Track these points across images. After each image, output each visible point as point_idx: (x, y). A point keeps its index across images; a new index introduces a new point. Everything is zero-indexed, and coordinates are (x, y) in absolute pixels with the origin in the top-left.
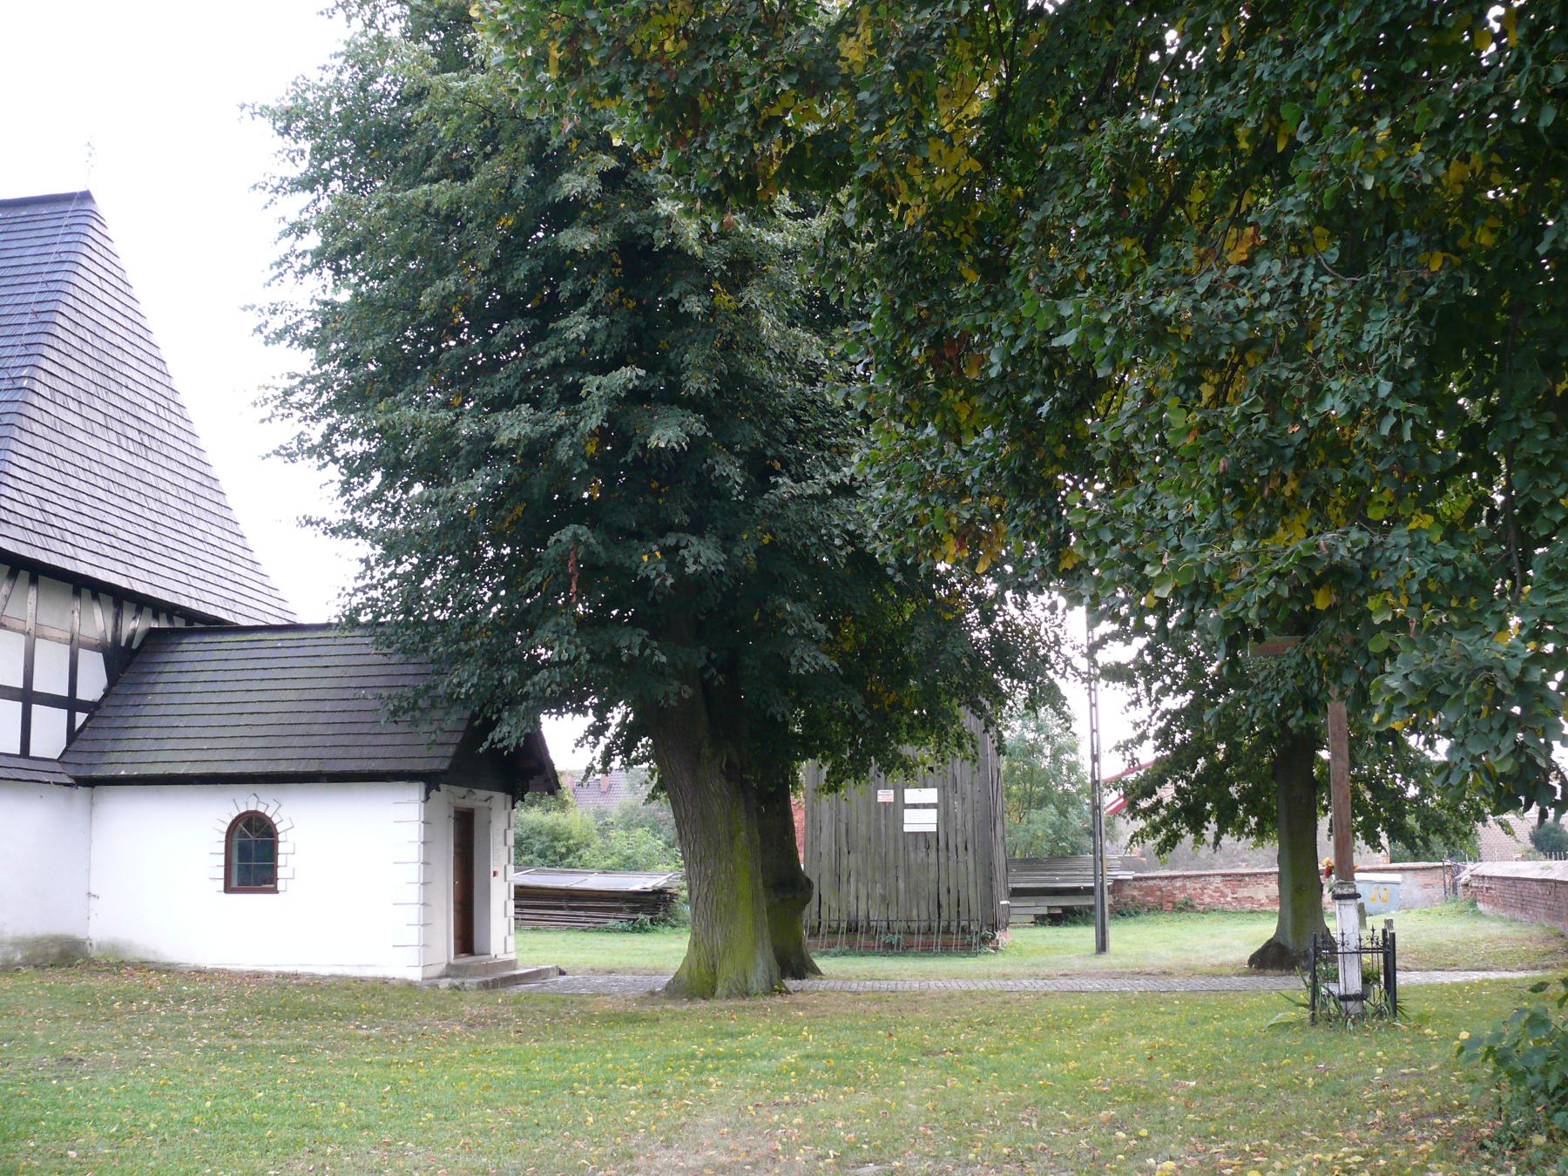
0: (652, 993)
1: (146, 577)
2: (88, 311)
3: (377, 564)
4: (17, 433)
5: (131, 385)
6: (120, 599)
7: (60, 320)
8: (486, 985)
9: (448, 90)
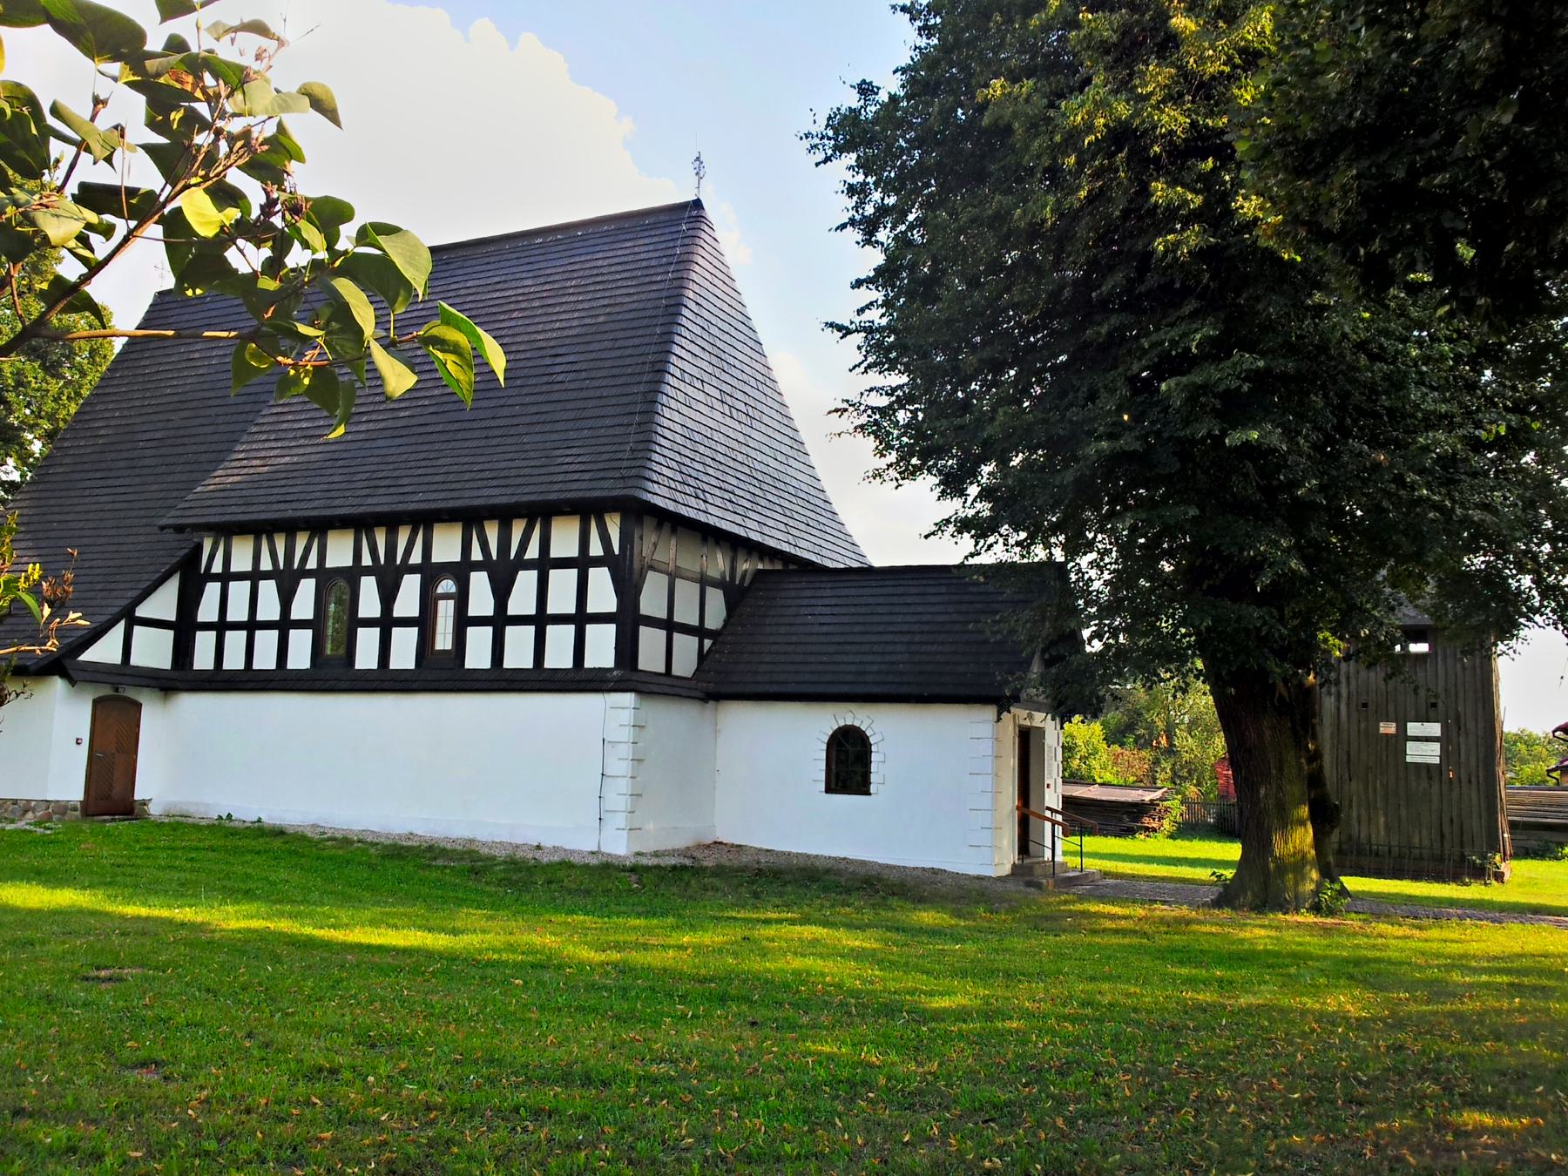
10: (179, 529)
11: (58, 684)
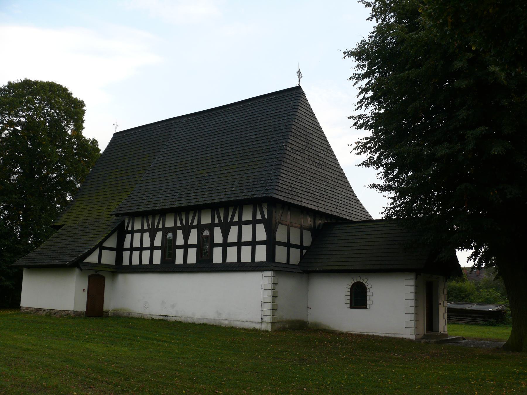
0: (498, 348)
1: (323, 206)
2: (301, 123)
3: (398, 199)
4: (282, 163)
5: (316, 145)
6: (315, 214)
7: (294, 127)
8: (437, 342)
9: (412, 38)
10: (117, 215)
11: (77, 271)
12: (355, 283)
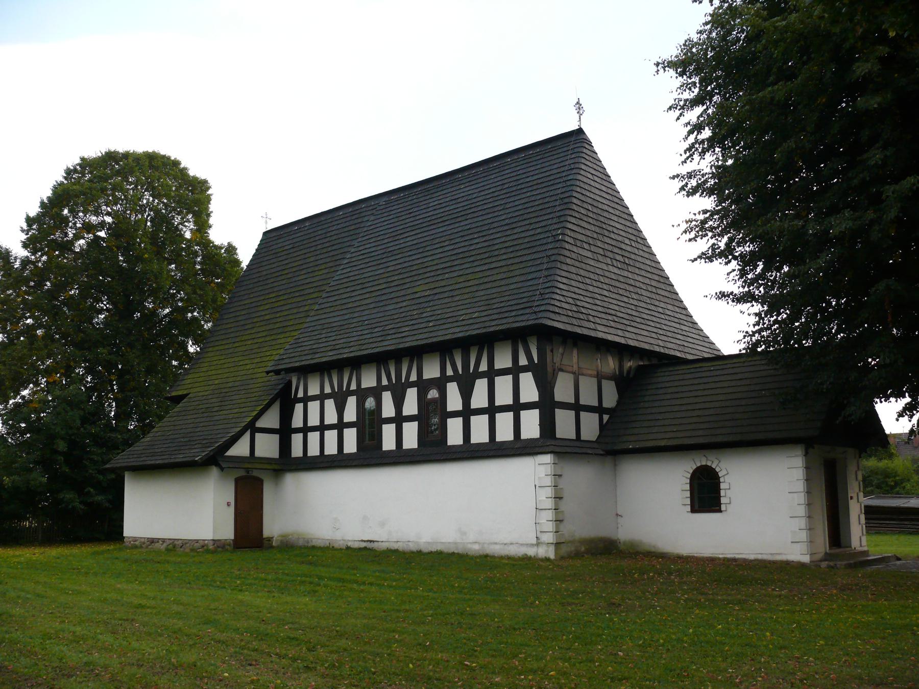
1: (634, 336)
2: (588, 194)
3: (766, 316)
4: (559, 265)
5: (615, 231)
7: (575, 201)
8: (850, 566)
9: (776, 28)
10: (277, 372)
11: (215, 471)
12: (706, 466)
